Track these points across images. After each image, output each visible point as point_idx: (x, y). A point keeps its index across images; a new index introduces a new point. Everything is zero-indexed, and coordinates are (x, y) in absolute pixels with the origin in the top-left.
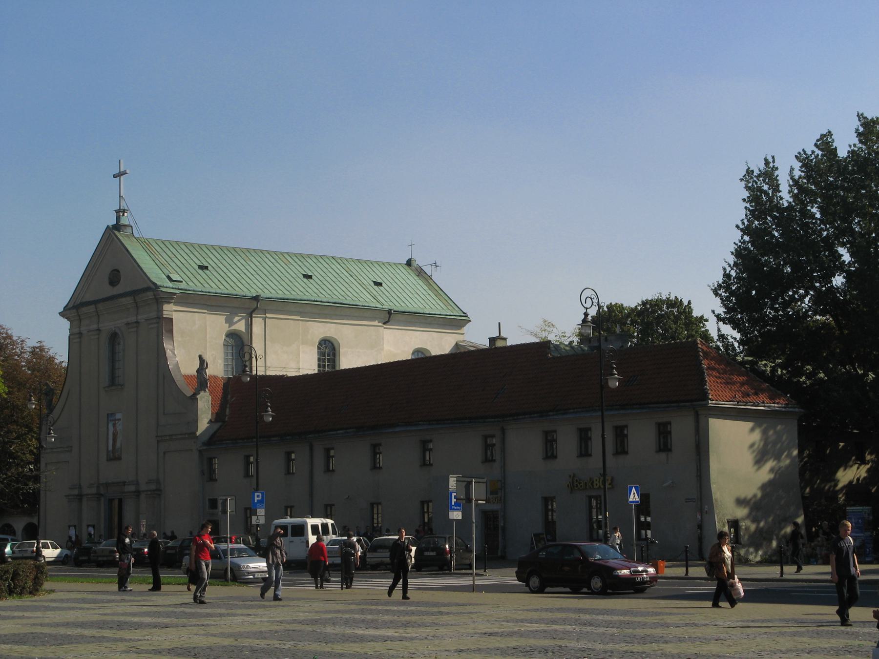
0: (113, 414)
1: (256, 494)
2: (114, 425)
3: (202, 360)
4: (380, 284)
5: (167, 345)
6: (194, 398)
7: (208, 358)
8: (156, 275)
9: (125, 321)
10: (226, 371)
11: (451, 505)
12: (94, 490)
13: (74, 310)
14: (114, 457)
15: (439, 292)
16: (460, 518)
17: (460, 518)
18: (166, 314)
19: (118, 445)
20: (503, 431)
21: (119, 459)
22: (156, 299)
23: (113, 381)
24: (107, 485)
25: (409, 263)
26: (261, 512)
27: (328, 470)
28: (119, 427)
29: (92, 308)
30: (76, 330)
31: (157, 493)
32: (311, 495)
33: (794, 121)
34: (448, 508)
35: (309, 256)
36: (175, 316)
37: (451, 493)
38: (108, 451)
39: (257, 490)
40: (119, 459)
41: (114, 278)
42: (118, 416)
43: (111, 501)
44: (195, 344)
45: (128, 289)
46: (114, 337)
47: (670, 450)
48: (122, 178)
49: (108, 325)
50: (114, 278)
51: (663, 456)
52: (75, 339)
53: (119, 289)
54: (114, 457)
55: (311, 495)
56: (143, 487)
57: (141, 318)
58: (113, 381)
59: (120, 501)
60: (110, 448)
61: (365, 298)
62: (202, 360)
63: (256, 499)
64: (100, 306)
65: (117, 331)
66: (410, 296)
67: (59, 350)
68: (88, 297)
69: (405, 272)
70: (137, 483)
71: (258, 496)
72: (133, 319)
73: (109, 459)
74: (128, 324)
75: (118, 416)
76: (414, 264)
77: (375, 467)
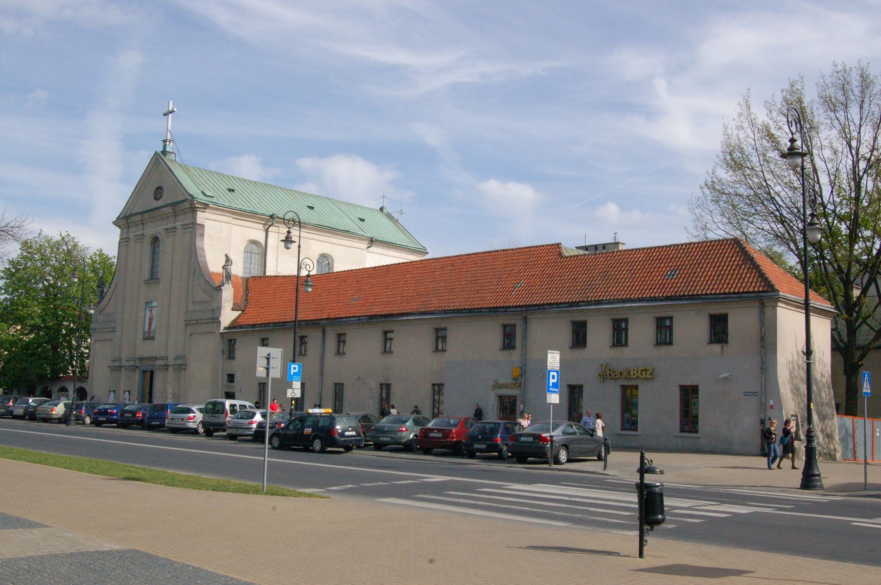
0: (151, 302)
1: (293, 366)
2: (151, 311)
3: (228, 259)
4: (363, 220)
5: (198, 244)
6: (219, 289)
7: (231, 256)
8: (193, 189)
9: (165, 227)
10: (245, 272)
11: (549, 387)
12: (131, 363)
13: (125, 221)
14: (149, 337)
15: (404, 230)
16: (557, 401)
17: (557, 401)
18: (199, 221)
19: (153, 327)
20: (525, 320)
21: (153, 338)
22: (192, 208)
23: (153, 277)
24: (142, 359)
25: (381, 209)
26: (297, 385)
27: (339, 353)
28: (155, 312)
29: (138, 218)
30: (126, 236)
31: (181, 367)
32: (322, 374)
33: (822, 46)
34: (544, 389)
35: (310, 195)
36: (207, 224)
37: (549, 371)
38: (144, 333)
39: (294, 361)
40: (153, 338)
41: (158, 192)
42: (154, 304)
43: (144, 372)
44: (223, 243)
45: (169, 202)
46: (155, 240)
47: (726, 342)
48: (170, 115)
49: (150, 230)
50: (158, 192)
51: (717, 347)
52: (124, 242)
53: (160, 203)
54: (149, 337)
55: (322, 374)
56: (171, 362)
57: (178, 224)
58: (153, 277)
59: (152, 372)
60: (147, 329)
61: (353, 227)
62: (228, 259)
63: (293, 371)
64: (146, 216)
65: (158, 235)
66: (385, 230)
67: (111, 250)
68: (136, 210)
69: (379, 215)
70: (166, 358)
71: (295, 368)
72: (170, 226)
73: (145, 339)
74: (166, 229)
75: (154, 304)
76: (385, 211)
77: (386, 351)
